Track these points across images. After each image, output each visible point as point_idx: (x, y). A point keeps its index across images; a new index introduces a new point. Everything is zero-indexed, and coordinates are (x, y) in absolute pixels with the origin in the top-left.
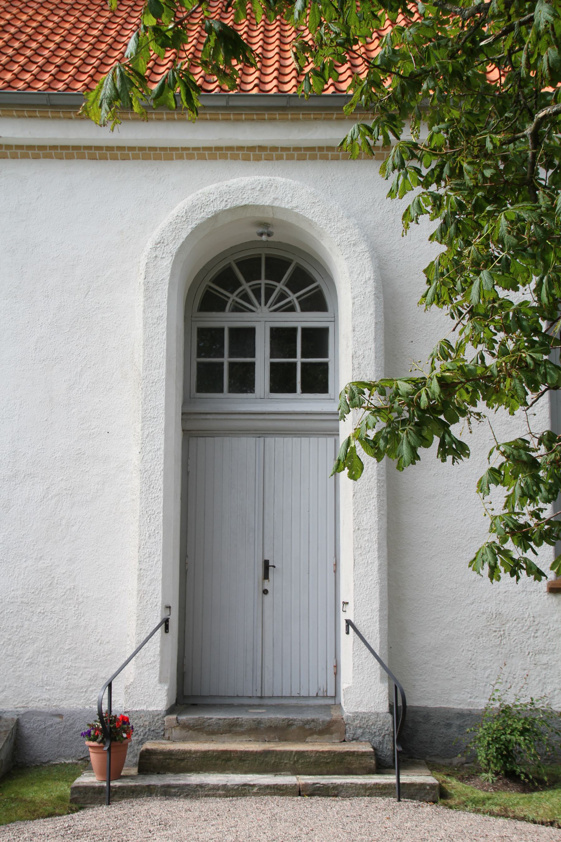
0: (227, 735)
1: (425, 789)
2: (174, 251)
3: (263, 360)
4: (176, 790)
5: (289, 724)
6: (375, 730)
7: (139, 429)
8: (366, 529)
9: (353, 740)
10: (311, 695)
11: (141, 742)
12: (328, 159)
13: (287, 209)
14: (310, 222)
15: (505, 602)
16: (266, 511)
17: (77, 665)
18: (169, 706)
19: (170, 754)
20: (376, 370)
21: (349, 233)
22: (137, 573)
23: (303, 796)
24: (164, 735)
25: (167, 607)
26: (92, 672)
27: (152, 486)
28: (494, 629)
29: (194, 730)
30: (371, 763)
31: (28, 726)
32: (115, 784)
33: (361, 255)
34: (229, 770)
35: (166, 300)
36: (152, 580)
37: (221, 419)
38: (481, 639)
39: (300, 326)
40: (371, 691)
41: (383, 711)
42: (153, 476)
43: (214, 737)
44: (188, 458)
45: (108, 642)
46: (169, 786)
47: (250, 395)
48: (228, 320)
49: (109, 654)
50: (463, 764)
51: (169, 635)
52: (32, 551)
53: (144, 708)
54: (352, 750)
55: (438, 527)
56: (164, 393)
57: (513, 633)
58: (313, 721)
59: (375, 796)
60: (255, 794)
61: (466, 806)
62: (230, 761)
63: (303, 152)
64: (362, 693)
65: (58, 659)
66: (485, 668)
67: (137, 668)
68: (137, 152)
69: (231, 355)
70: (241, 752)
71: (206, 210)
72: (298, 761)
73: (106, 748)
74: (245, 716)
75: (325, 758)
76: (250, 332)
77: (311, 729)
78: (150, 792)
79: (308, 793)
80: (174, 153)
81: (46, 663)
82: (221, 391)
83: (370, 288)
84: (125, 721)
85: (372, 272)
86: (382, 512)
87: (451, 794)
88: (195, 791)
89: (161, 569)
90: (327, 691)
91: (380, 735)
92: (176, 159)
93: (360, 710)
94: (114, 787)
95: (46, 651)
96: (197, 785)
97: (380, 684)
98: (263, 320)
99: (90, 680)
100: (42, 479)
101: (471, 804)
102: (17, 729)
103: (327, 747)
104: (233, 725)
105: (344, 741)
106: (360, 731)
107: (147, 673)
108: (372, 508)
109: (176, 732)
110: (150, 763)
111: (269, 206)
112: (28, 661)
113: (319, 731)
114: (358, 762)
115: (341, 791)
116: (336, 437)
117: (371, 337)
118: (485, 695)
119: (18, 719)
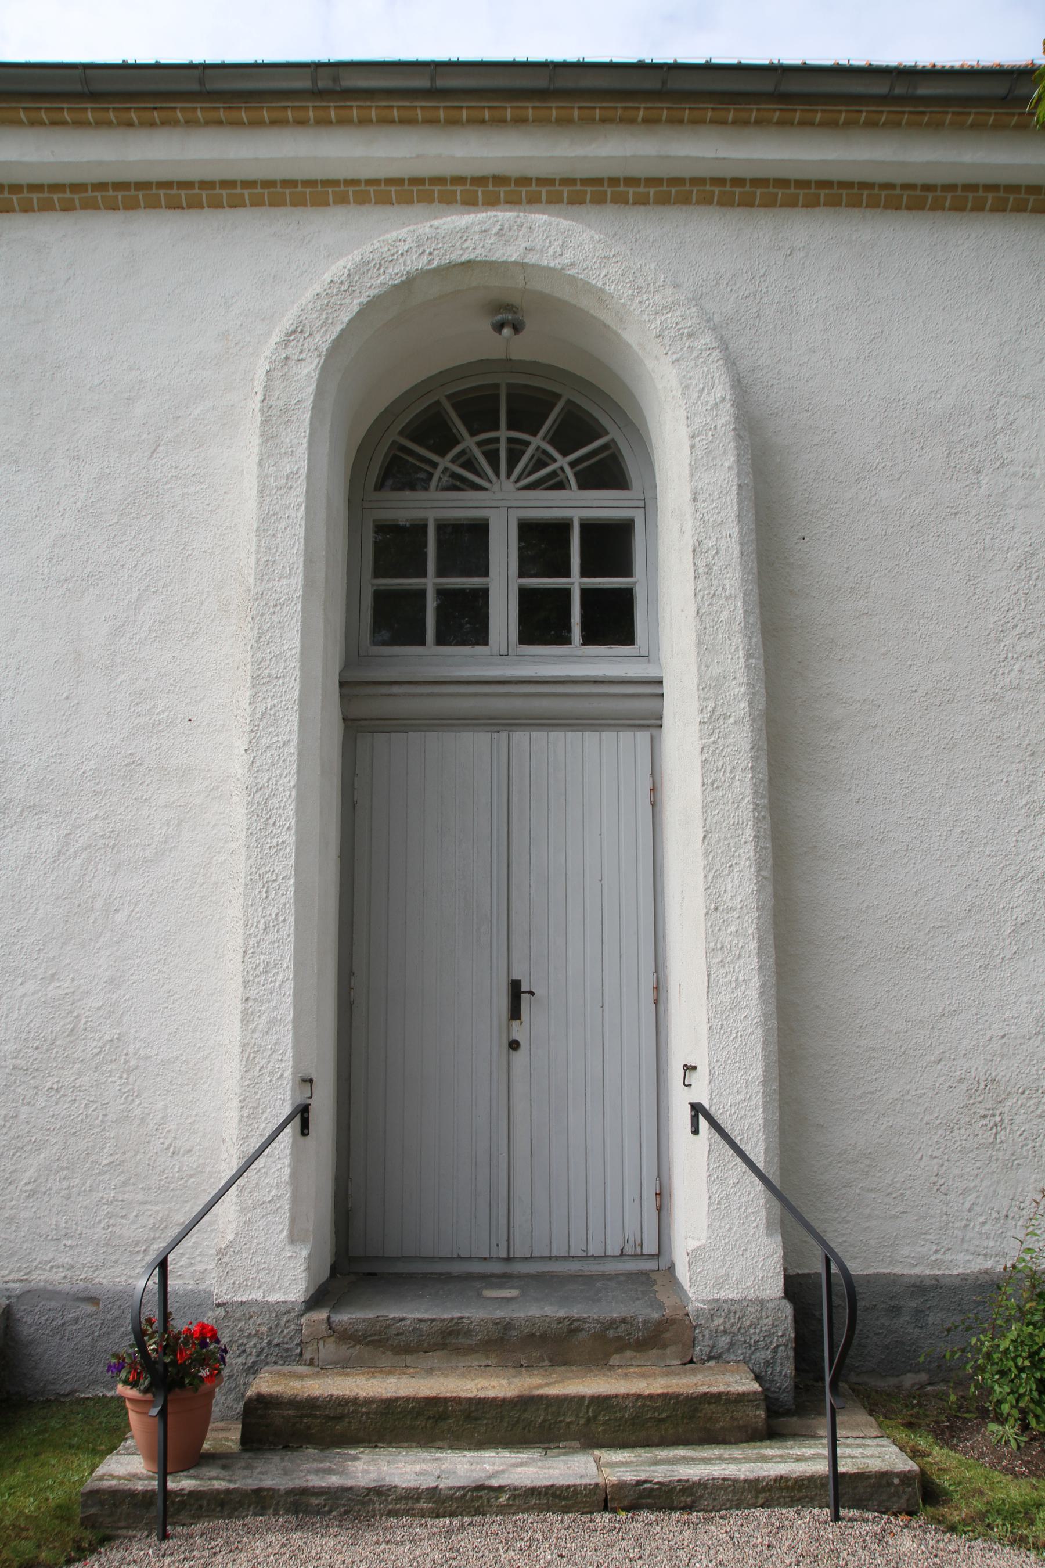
0: (438, 1353)
1: (890, 1484)
2: (324, 347)
3: (503, 583)
4: (320, 1500)
5: (572, 1329)
6: (755, 1338)
7: (245, 703)
8: (732, 909)
9: (710, 1358)
10: (609, 1253)
11: (253, 1370)
12: (627, 203)
13: (553, 269)
14: (599, 295)
15: (1003, 1056)
16: (514, 881)
17: (126, 1196)
18: (312, 1291)
19: (311, 1405)
20: (742, 579)
21: (678, 313)
22: (240, 1006)
23: (614, 1511)
24: (301, 1354)
25: (304, 1081)
26: (158, 1212)
27: (271, 822)
28: (982, 1112)
29: (367, 1344)
30: (756, 1416)
31: (29, 1319)
32: (181, 1483)
33: (704, 354)
34: (443, 1439)
35: (305, 441)
36: (272, 1022)
37: (422, 695)
38: (956, 1133)
39: (576, 516)
40: (747, 1254)
41: (773, 1296)
42: (274, 800)
43: (409, 1359)
44: (355, 774)
45: (189, 1151)
46: (305, 1492)
47: (479, 649)
48: (434, 506)
49: (191, 1176)
50: (922, 1387)
51: (310, 1141)
52: (35, 964)
53: (257, 1295)
54: (715, 1389)
55: (868, 907)
56: (298, 627)
57: (1018, 1119)
58: (624, 1321)
59: (779, 1505)
60: (504, 1510)
61: (990, 1526)
62: (445, 1419)
63: (578, 188)
64: (721, 1249)
65: (88, 1184)
66: (966, 1192)
67: (241, 1211)
68: (259, 190)
69: (441, 573)
70: (470, 1400)
71: (390, 270)
72: (595, 1417)
73: (154, 1411)
74: (474, 1313)
75: (655, 1409)
76: (480, 530)
77: (619, 1338)
78: (260, 1501)
79: (626, 1503)
80: (330, 190)
81: (64, 1192)
82: (422, 642)
83: (725, 416)
84: (207, 1335)
85: (728, 388)
86: (764, 873)
87: (946, 1493)
88: (363, 1503)
89: (290, 1000)
90: (641, 1245)
91: (766, 1347)
92: (335, 203)
93: (723, 1294)
94: (179, 1493)
95: (63, 1168)
96: (369, 1489)
97: (766, 1240)
98: (504, 507)
99: (154, 1228)
100: (56, 816)
101: (999, 1521)
102: (7, 1327)
103: (657, 1385)
104: (450, 1333)
105: (691, 1361)
106: (724, 1341)
107: (263, 1222)
108: (744, 863)
109: (328, 1350)
110: (273, 1427)
111: (515, 263)
112: (29, 1188)
113: (638, 1341)
114: (728, 1416)
115: (701, 1497)
116: (655, 731)
117: (731, 511)
118: (965, 1246)
119: (9, 1306)
